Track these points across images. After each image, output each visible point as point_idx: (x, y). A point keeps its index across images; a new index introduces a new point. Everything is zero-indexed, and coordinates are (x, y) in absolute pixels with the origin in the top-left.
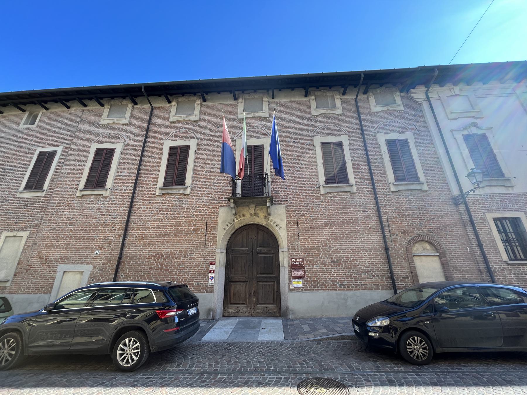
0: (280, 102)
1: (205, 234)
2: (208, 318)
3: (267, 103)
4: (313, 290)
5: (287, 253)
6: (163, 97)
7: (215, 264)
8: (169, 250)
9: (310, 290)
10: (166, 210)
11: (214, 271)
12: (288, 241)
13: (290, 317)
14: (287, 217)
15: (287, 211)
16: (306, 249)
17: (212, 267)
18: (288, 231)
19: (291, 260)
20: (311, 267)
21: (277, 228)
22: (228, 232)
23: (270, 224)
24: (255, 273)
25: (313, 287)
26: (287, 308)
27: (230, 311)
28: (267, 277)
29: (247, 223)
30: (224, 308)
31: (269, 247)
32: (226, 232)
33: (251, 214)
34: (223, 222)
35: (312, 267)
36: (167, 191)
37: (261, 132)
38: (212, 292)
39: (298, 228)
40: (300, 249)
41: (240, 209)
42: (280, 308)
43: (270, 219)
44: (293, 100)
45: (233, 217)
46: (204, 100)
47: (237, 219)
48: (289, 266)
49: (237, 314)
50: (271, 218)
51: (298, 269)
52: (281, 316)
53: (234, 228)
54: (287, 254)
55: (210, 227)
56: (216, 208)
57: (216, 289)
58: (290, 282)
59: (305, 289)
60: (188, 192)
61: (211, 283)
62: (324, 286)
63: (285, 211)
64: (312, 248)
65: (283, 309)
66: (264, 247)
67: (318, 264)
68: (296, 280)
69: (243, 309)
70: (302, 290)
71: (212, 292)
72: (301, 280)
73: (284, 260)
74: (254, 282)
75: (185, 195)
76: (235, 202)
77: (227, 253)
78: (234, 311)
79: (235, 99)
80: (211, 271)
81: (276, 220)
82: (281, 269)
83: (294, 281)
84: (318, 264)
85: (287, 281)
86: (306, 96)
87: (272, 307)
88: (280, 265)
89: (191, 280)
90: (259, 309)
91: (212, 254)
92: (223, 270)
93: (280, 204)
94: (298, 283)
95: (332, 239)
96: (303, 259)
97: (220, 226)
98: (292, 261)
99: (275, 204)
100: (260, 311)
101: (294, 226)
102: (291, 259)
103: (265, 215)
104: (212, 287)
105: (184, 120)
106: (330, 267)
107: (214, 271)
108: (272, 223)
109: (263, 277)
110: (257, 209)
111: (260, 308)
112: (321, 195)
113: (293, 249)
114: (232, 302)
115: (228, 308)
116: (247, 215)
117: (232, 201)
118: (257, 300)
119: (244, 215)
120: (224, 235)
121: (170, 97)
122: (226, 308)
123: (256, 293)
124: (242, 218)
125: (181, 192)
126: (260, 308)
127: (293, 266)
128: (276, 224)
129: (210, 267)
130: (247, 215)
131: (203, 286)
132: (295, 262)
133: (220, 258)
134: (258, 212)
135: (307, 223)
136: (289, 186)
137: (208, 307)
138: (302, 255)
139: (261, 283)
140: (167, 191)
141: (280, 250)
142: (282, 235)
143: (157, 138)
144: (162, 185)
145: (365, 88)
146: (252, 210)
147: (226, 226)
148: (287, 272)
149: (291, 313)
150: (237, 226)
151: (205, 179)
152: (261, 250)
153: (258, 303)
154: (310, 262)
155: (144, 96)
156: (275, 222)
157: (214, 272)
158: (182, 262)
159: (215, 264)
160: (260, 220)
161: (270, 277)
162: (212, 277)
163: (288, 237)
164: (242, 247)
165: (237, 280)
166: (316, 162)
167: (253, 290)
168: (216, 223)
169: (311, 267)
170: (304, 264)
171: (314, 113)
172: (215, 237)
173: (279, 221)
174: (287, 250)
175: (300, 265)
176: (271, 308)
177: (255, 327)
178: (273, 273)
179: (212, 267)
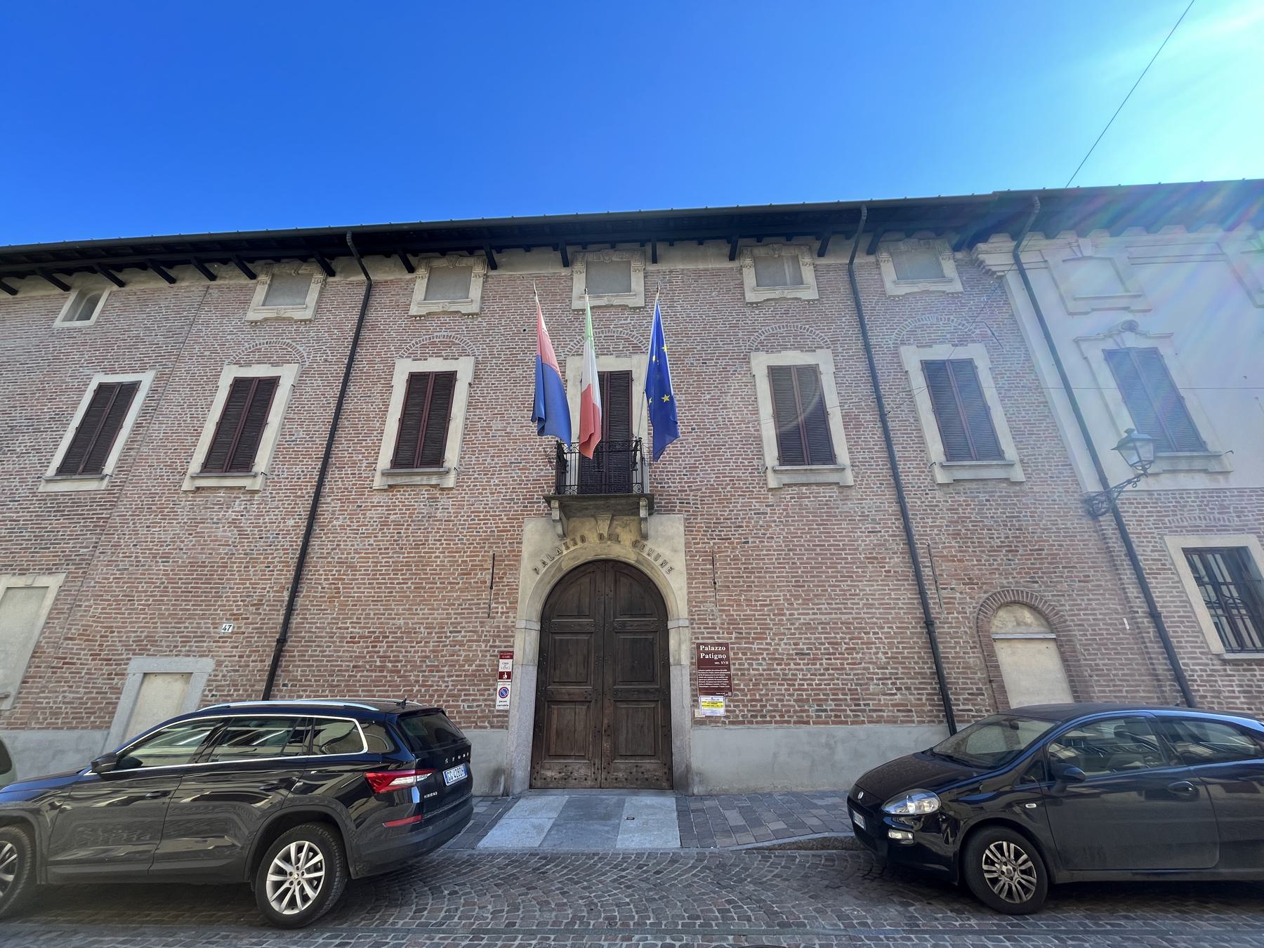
0: (671, 272)
1: (488, 584)
2: (494, 793)
3: (641, 275)
4: (751, 723)
5: (686, 630)
6: (396, 259)
7: (512, 657)
8: (402, 621)
9: (743, 723)
10: (397, 524)
11: (509, 675)
12: (689, 601)
13: (695, 791)
14: (687, 544)
15: (689, 529)
16: (733, 622)
17: (505, 665)
18: (690, 578)
19: (698, 648)
20: (746, 666)
21: (664, 570)
22: (547, 580)
23: (645, 559)
24: (611, 680)
25: (751, 715)
26: (688, 768)
27: (549, 774)
28: (639, 691)
29: (590, 558)
30: (532, 767)
31: (644, 615)
32: (542, 579)
33: (601, 537)
34: (534, 555)
35: (748, 666)
36: (399, 480)
37: (626, 340)
38: (503, 726)
39: (714, 571)
40: (718, 621)
41: (575, 523)
42: (671, 769)
43: (647, 549)
44: (701, 266)
45: (557, 543)
46: (493, 266)
47: (567, 548)
48: (692, 664)
49: (563, 783)
50: (649, 544)
51: (713, 670)
52: (672, 787)
53: (560, 569)
54: (686, 634)
55: (501, 566)
56: (516, 522)
57: (514, 721)
58: (695, 703)
59: (731, 720)
60: (450, 481)
61: (501, 703)
62: (777, 715)
63: (682, 529)
64: (747, 618)
65: (678, 769)
66: (632, 616)
67: (764, 659)
68: (709, 698)
69: (580, 769)
70: (724, 723)
71: (503, 726)
72: (721, 699)
73: (681, 648)
74: (607, 703)
75: (443, 489)
76: (562, 508)
77: (542, 631)
78: (558, 776)
79: (566, 263)
80: (501, 674)
81: (660, 550)
82: (674, 671)
83: (704, 699)
84: (764, 659)
85: (688, 701)
86: (732, 258)
87: (650, 765)
88: (671, 660)
89: (453, 696)
90: (617, 770)
91: (507, 633)
92: (532, 672)
93: (671, 511)
94: (713, 706)
95: (797, 597)
96: (726, 645)
97: (526, 564)
98: (699, 652)
99: (659, 512)
100: (620, 775)
101: (705, 565)
102: (699, 645)
103: (634, 539)
104: (505, 714)
105: (445, 313)
106: (792, 666)
107: (509, 675)
108: (651, 559)
109: (628, 691)
110: (615, 523)
111: (622, 766)
112: (771, 490)
113: (703, 621)
114: (552, 752)
115: (542, 767)
116: (592, 538)
117: (555, 504)
118: (615, 747)
119: (583, 539)
120: (536, 587)
121: (411, 258)
122: (538, 768)
123: (612, 731)
124: (580, 544)
125: (434, 482)
126: (622, 767)
127: (703, 664)
128: (660, 561)
129: (501, 665)
130: (592, 538)
131: (483, 711)
132: (707, 653)
133: (526, 643)
134: (619, 530)
135: (736, 559)
136: (693, 468)
137: (493, 765)
138: (723, 637)
139: (624, 706)
140: (399, 480)
141: (670, 624)
142: (677, 589)
143: (379, 354)
144: (389, 466)
145: (870, 239)
146: (604, 527)
147: (540, 566)
148: (687, 678)
149: (697, 779)
150: (567, 565)
151: (492, 451)
152: (624, 624)
153: (615, 754)
154: (744, 654)
155: (351, 254)
156: (658, 556)
157: (509, 677)
158: (433, 651)
159: (512, 657)
160: (623, 551)
161: (646, 691)
162: (506, 690)
163: (690, 593)
164: (579, 616)
165: (566, 698)
166: (756, 412)
167: (606, 721)
168: (517, 556)
169: (746, 666)
170: (728, 659)
171: (751, 297)
172: (513, 590)
173: (668, 552)
174: (687, 623)
175: (719, 660)
176: (648, 766)
177: (609, 816)
178: (653, 681)
179: (505, 665)
